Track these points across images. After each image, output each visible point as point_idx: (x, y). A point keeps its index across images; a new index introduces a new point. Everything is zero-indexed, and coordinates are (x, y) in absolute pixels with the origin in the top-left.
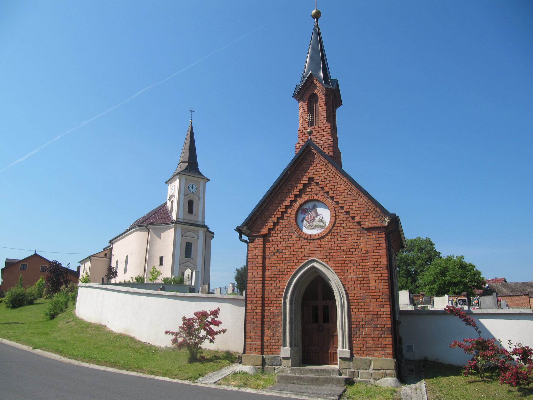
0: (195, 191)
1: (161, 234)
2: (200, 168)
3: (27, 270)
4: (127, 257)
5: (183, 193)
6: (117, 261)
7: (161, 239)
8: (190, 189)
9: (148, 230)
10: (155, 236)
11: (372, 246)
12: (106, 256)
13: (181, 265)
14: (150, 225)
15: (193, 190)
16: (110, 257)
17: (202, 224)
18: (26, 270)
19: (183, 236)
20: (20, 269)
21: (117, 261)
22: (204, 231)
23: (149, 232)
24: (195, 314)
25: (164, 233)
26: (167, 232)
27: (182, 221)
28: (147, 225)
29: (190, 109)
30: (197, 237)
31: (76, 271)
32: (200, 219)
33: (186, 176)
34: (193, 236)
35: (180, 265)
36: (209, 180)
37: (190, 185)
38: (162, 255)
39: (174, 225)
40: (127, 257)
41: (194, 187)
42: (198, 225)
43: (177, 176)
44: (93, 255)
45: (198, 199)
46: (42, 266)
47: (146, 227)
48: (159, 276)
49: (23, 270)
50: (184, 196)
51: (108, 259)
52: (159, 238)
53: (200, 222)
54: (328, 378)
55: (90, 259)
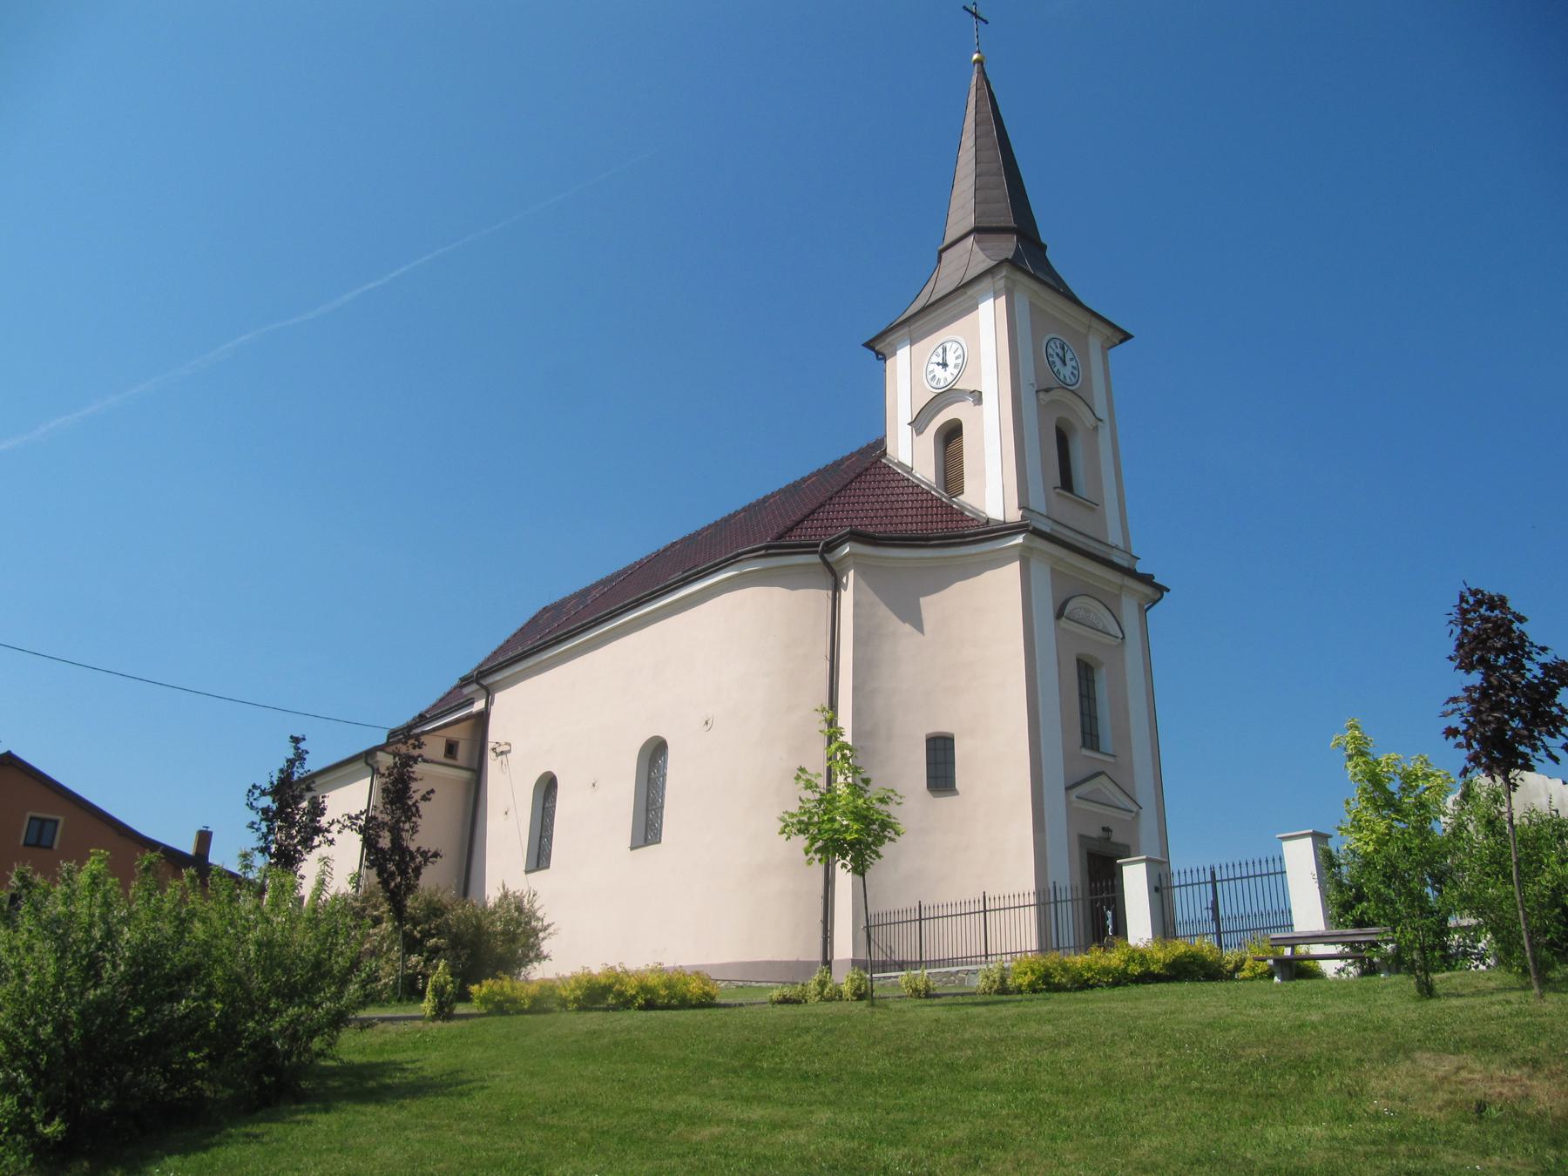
1: (923, 601)
3: (56, 846)
4: (655, 752)
5: (1028, 375)
6: (547, 787)
7: (927, 627)
9: (830, 580)
10: (883, 611)
12: (454, 758)
14: (856, 541)
16: (476, 766)
18: (50, 847)
20: (22, 842)
21: (547, 787)
23: (837, 587)
26: (958, 586)
28: (831, 547)
32: (1114, 537)
35: (1068, 789)
36: (1126, 337)
38: (943, 727)
39: (1019, 540)
40: (655, 752)
41: (1069, 356)
43: (987, 283)
46: (32, 818)
47: (822, 557)
48: (426, 888)
49: (38, 845)
50: (1037, 392)
51: (465, 775)
52: (907, 628)
54: (18, 1101)
55: (367, 764)
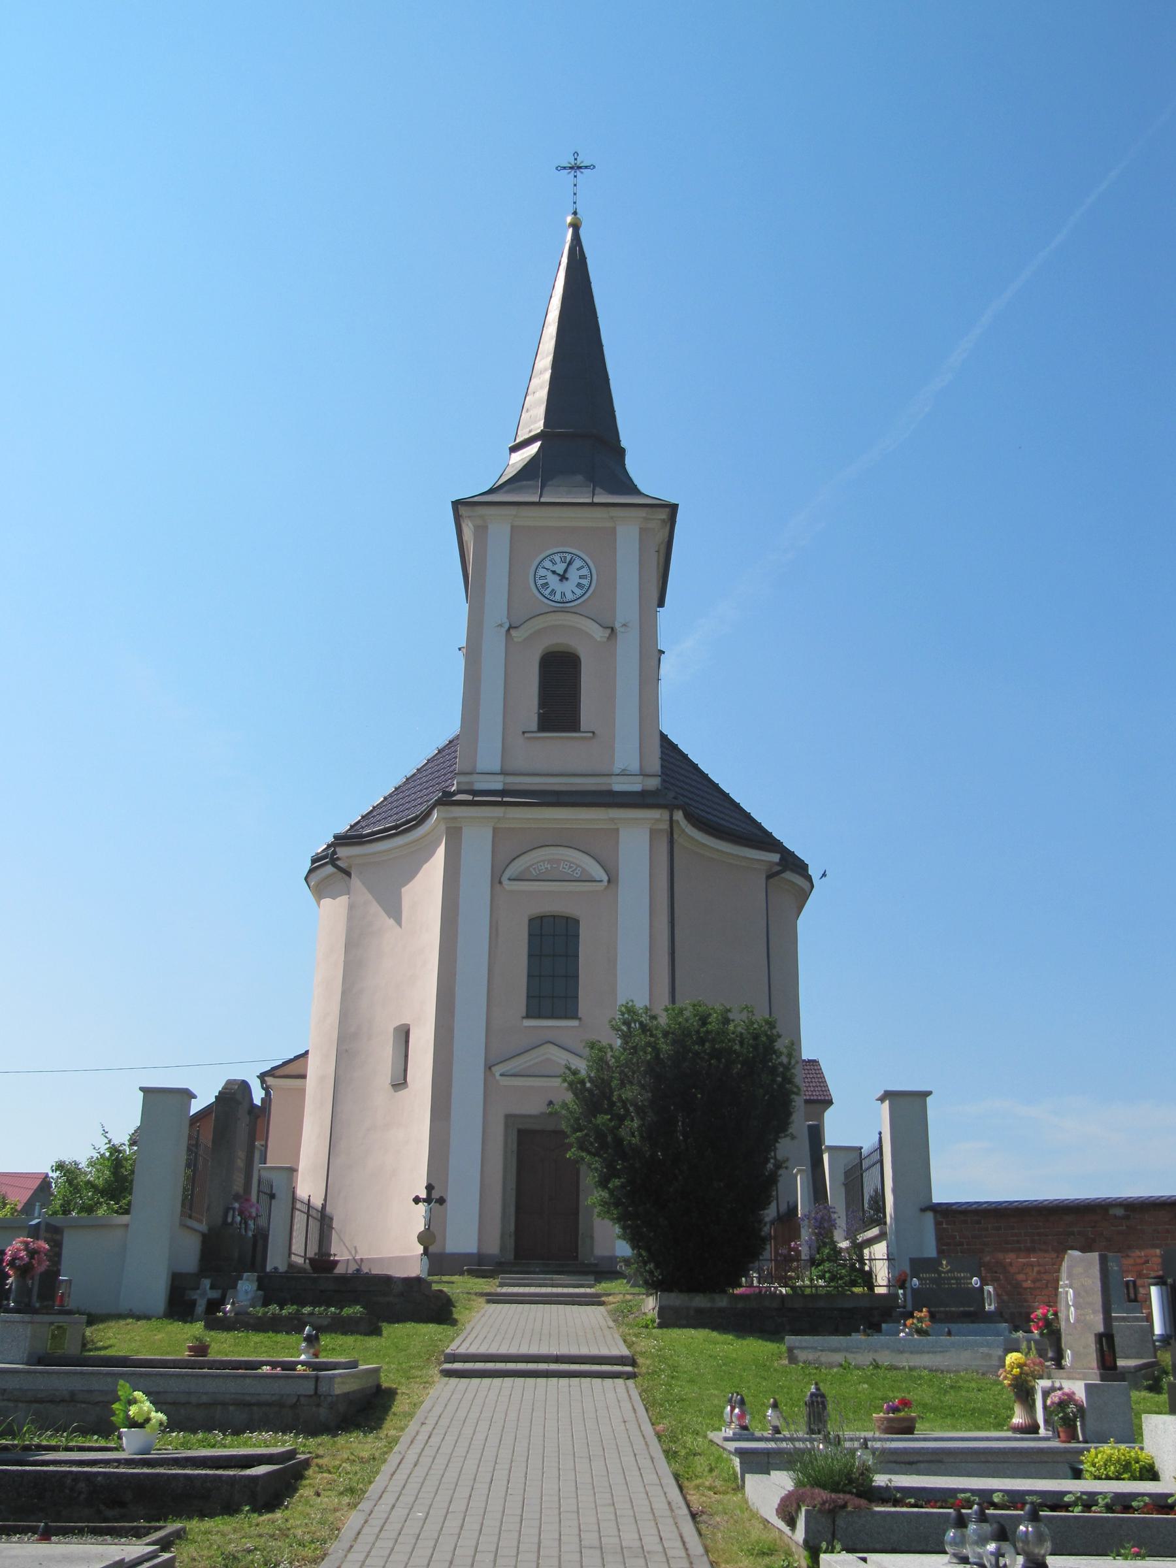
0: (579, 592)
2: (634, 466)
5: (497, 611)
8: (546, 585)
10: (375, 908)
11: (590, 1538)
13: (497, 1070)
15: (569, 588)
17: (637, 788)
19: (505, 882)
22: (653, 833)
24: (60, 1166)
25: (416, 878)
27: (497, 784)
29: (568, 160)
30: (598, 872)
31: (748, 1473)
33: (512, 510)
34: (577, 874)
35: (489, 1068)
37: (547, 564)
42: (611, 793)
44: (274, 1069)
45: (599, 634)
52: (391, 922)
53: (624, 773)
